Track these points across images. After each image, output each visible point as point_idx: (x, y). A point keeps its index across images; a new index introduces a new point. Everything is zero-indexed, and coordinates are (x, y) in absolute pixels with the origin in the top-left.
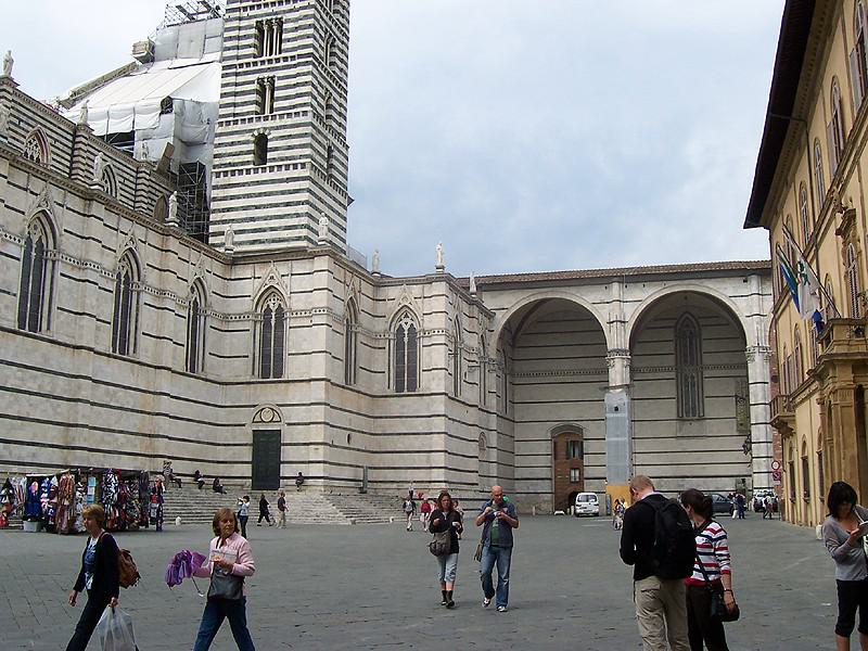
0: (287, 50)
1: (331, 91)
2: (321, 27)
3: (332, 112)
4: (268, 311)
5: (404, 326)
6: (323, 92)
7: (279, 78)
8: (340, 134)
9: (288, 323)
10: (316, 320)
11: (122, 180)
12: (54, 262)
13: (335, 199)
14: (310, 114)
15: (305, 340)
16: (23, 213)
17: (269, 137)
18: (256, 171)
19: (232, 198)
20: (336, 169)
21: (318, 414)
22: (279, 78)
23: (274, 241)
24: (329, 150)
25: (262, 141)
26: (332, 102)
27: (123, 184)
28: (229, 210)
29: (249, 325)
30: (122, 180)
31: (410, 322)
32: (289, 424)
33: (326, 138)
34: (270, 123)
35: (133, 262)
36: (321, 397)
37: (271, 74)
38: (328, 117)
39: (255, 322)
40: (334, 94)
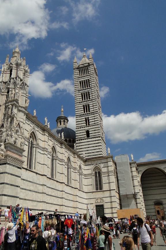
5: (97, 171)
7: (90, 117)
18: (87, 139)
22: (90, 117)
25: (88, 133)
34: (89, 128)
37: (88, 117)
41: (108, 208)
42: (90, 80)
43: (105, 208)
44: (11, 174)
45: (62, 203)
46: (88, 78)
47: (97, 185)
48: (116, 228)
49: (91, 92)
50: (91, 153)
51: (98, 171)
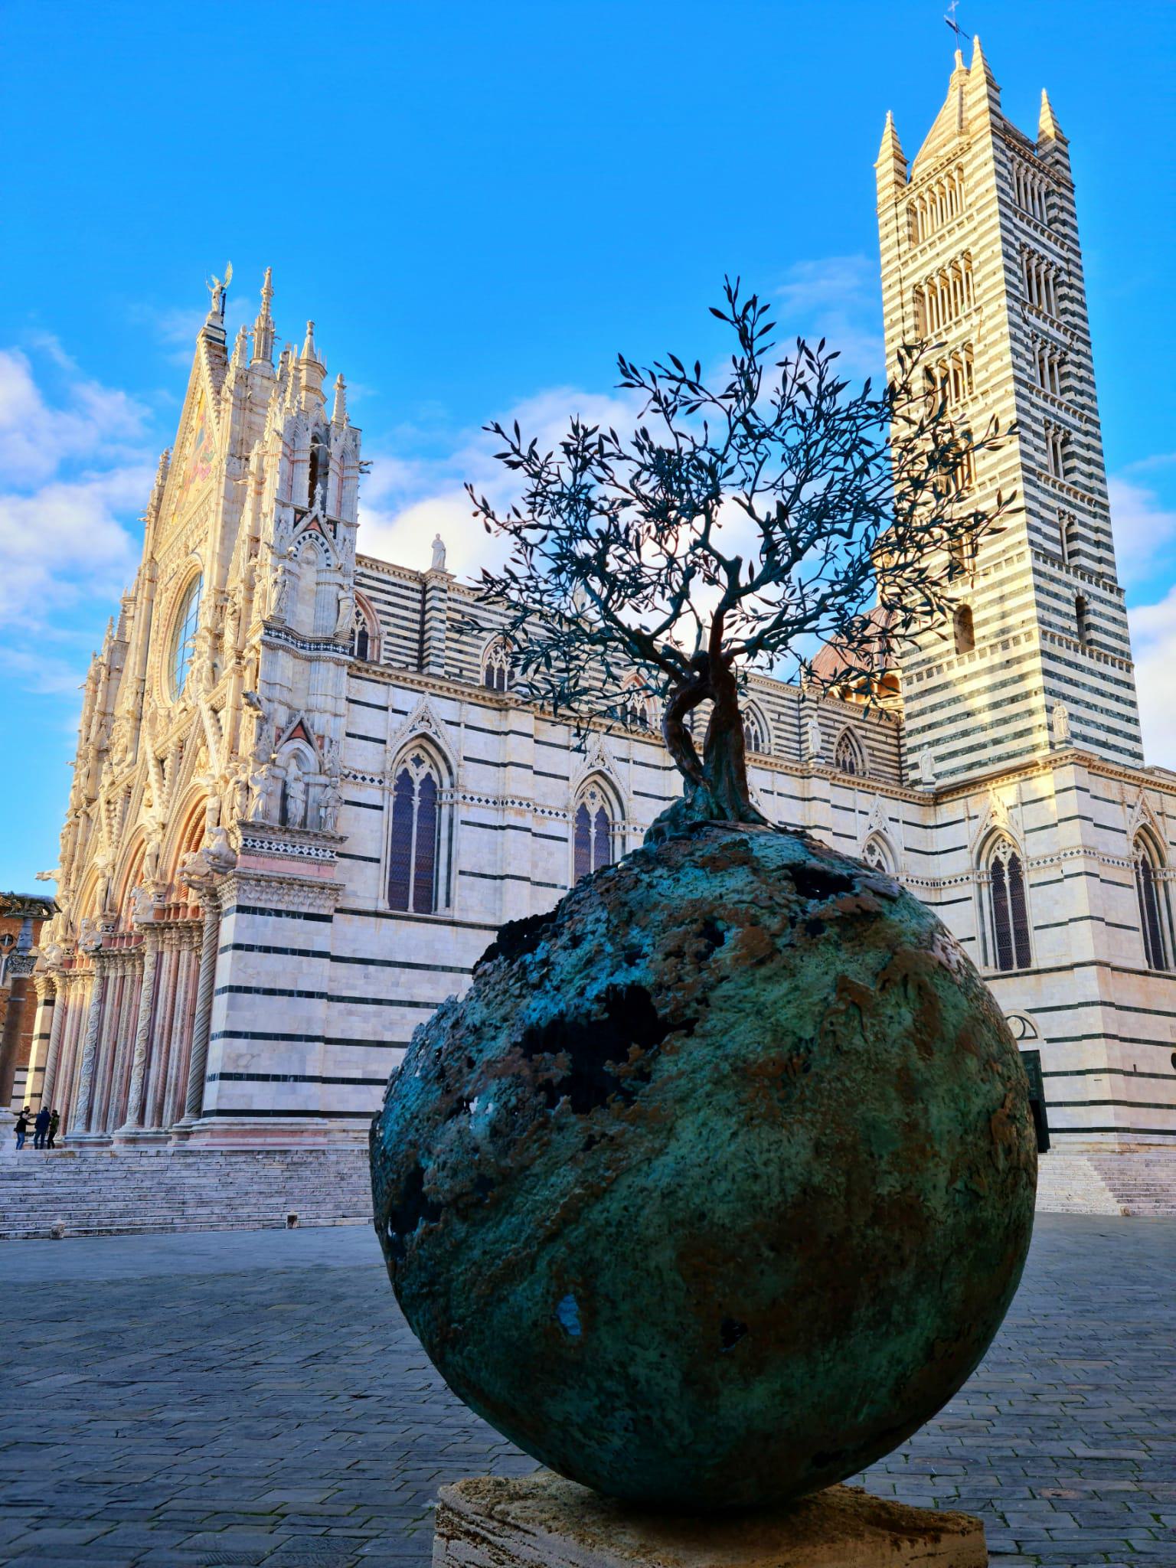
0: (983, 473)
1: (1073, 512)
2: (1035, 420)
3: (1078, 545)
4: (998, 865)
5: (1001, 857)
6: (1055, 518)
8: (1101, 575)
9: (1028, 878)
10: (1070, 867)
11: (776, 716)
12: (624, 838)
13: (1104, 677)
14: (1029, 556)
15: (1057, 903)
16: (1124, 832)
17: (973, 608)
19: (933, 708)
20: (1097, 628)
21: (1092, 1020)
23: (1000, 759)
24: (1080, 604)
26: (1077, 529)
27: (778, 721)
28: (930, 727)
29: (970, 890)
30: (776, 716)
31: (1010, 851)
32: (1050, 1041)
33: (1068, 585)
35: (1150, 843)
36: (1094, 992)
38: (1073, 554)
39: (980, 885)
40: (1080, 516)
41: (1065, 1074)
42: (973, 251)
43: (1046, 1075)
44: (267, 950)
45: (498, 892)
46: (963, 246)
47: (1002, 937)
48: (434, 783)
49: (979, 341)
50: (983, 746)
51: (1009, 856)
